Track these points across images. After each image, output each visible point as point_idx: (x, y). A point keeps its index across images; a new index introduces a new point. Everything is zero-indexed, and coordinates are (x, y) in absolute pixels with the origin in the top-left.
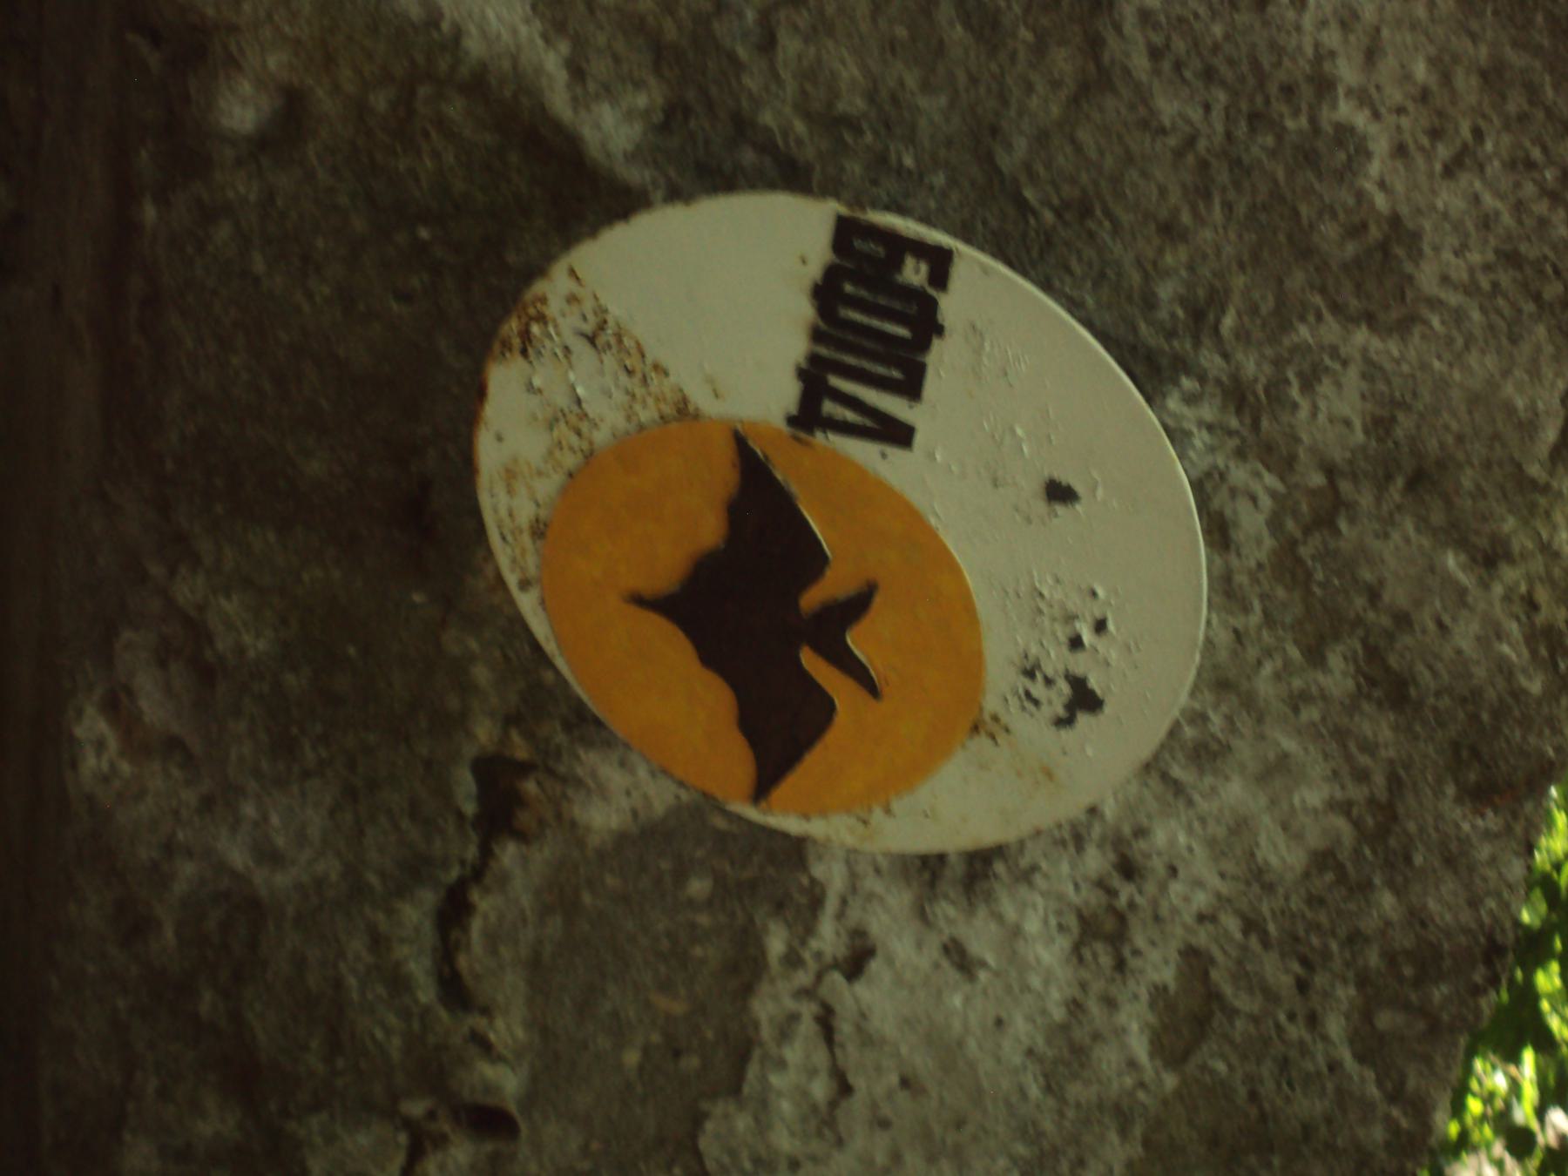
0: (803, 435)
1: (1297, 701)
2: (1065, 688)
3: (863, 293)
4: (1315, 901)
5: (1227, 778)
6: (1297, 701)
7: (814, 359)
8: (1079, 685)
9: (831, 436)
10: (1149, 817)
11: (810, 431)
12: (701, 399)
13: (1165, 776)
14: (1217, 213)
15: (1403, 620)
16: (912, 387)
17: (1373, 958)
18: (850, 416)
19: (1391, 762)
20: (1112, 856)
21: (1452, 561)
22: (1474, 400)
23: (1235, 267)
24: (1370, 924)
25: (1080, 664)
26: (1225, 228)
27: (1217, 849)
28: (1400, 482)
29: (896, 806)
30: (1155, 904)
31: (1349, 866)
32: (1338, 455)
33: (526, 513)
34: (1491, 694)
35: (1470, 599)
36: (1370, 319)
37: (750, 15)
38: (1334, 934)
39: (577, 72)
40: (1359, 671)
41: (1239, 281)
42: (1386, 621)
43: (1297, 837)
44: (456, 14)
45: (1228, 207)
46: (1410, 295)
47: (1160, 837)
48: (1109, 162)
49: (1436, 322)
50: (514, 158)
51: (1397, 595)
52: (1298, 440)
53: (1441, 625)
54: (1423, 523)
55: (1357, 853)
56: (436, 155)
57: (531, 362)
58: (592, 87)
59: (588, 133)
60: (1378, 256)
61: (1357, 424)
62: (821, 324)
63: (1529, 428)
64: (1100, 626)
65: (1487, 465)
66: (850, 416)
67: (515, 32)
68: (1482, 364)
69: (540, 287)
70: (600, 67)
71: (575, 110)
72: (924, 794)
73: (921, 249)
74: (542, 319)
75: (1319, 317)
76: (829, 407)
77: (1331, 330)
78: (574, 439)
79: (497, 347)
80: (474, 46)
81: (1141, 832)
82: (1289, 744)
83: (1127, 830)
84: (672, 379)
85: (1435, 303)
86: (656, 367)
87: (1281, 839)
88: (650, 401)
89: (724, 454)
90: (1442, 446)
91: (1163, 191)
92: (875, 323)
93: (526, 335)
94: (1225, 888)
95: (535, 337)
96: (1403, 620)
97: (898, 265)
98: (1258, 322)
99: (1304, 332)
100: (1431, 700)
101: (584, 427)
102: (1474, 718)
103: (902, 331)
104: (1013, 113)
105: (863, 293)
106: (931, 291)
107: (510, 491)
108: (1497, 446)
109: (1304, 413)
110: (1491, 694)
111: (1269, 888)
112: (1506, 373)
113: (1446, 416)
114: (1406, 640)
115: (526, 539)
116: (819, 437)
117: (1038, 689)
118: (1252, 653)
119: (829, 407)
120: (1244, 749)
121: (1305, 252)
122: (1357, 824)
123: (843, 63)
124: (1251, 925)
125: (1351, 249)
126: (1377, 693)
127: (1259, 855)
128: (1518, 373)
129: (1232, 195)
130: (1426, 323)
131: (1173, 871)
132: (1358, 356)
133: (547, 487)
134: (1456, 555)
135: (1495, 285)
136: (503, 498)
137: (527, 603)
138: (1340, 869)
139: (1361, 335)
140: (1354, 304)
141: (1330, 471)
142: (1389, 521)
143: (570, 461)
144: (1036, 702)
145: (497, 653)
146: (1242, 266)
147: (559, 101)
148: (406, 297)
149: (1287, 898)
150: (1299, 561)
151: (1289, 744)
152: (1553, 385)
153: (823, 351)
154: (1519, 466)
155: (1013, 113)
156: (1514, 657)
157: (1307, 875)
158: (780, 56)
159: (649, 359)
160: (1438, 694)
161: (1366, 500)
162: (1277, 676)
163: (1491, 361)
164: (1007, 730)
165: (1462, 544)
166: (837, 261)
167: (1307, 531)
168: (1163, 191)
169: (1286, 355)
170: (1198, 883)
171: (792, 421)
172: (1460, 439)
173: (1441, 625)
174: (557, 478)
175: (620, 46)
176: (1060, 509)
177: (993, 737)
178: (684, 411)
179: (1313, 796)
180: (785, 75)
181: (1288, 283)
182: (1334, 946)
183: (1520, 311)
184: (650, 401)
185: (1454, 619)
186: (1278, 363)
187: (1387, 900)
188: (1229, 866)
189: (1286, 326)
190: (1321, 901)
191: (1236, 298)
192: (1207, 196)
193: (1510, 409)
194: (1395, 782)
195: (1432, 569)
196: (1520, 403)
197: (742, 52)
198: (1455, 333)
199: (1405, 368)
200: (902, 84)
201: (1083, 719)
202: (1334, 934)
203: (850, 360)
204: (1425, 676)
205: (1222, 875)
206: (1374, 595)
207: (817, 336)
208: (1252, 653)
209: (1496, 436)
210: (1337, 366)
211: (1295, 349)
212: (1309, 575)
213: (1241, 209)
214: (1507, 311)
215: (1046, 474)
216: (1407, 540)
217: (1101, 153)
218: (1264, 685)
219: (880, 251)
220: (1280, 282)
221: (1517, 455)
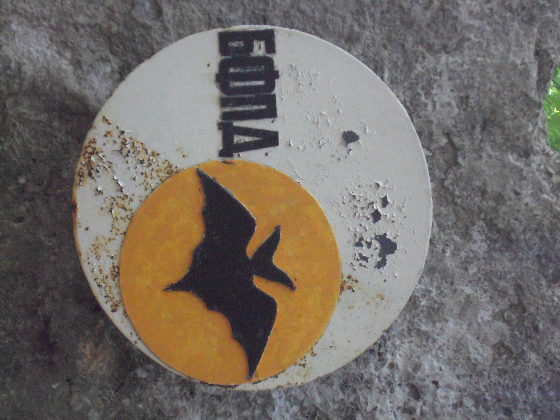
0: (228, 159)
1: (465, 264)
2: (376, 244)
3: (238, 70)
4: (503, 372)
5: (447, 321)
6: (465, 264)
7: (225, 116)
8: (382, 239)
9: (241, 154)
10: (418, 358)
11: (231, 156)
12: (179, 163)
13: (419, 332)
14: (369, 22)
15: (500, 199)
16: (271, 113)
17: (535, 394)
18: (247, 139)
19: (513, 279)
20: (407, 390)
21: (511, 158)
22: (498, 70)
23: (381, 48)
24: (529, 373)
25: (381, 228)
26: (373, 28)
27: (451, 363)
28: (478, 129)
29: (316, 351)
30: (433, 407)
31: (511, 346)
32: (449, 123)
33: (107, 265)
34: (546, 222)
35: (525, 174)
36: (445, 48)
37: (148, 5)
38: (515, 387)
39: (77, 63)
40: (488, 238)
41: (385, 53)
42: (491, 203)
43: (484, 340)
44: (16, 58)
45: (372, 15)
46: (459, 28)
47: (426, 366)
48: (317, 15)
49: (472, 36)
50: (56, 124)
51: (493, 187)
52: (431, 122)
53: (517, 193)
54: (494, 145)
55: (513, 336)
56: (20, 135)
57: (93, 178)
58: (85, 67)
59: (88, 93)
60: (441, 13)
61: (453, 103)
62: (224, 96)
63: (525, 74)
64: (385, 202)
65: (513, 100)
66: (247, 139)
67: (45, 55)
68: (498, 50)
69: (91, 135)
70: (86, 57)
71: (80, 84)
72: (327, 338)
73: (258, 35)
74: (95, 152)
75: (424, 57)
76: (238, 139)
77: (430, 61)
78: (123, 214)
79: (77, 178)
80: (28, 70)
81: (417, 367)
82: (468, 290)
83: (410, 370)
84: (162, 157)
85: (469, 28)
86: (153, 154)
87: (478, 344)
88: (155, 175)
89: (193, 182)
90: (491, 101)
91: (343, 19)
92: (248, 84)
93: (89, 164)
94: (460, 383)
95: (93, 162)
96: (500, 199)
97: (250, 48)
98: (399, 71)
99: (419, 68)
100: (522, 237)
101: (126, 203)
102: (542, 238)
103: (261, 83)
104: (271, 8)
105: (238, 70)
106: (269, 56)
107: (98, 257)
108: (515, 90)
109: (430, 107)
110: (546, 222)
111: (480, 374)
112: (508, 50)
113: (489, 85)
114: (503, 209)
115: (110, 282)
116: (236, 158)
117: (365, 252)
118: (440, 247)
119: (238, 139)
120: (449, 302)
121: (409, 24)
122: (508, 322)
123: (193, 11)
124: (479, 400)
125: (429, 14)
126: (498, 246)
127: (472, 357)
128: (513, 48)
129: (372, 9)
130: (469, 39)
131: (436, 383)
132: (445, 69)
133: (114, 247)
134: (512, 154)
135: (491, 10)
136: (92, 259)
137: (117, 318)
138: (509, 351)
139: (444, 58)
140: (437, 43)
141: (448, 135)
142: (479, 151)
143: (123, 226)
144: (366, 259)
145: (99, 400)
146: (385, 46)
147: (72, 84)
148: (20, 220)
149: (489, 377)
150: (447, 189)
151: (468, 290)
152: (529, 47)
153: (227, 110)
154: (526, 95)
155: (271, 8)
156: (551, 199)
157: (494, 360)
158: (165, 17)
159: (149, 152)
160: (524, 231)
161: (467, 143)
162: (453, 255)
163: (500, 46)
164: (356, 281)
165: (513, 148)
166: (223, 58)
167: (446, 173)
168: (343, 19)
169: (415, 81)
170: (449, 386)
171: (222, 154)
172: (498, 93)
173: (517, 193)
174: (119, 238)
175: (93, 45)
176: (351, 145)
177: (350, 288)
178: (171, 171)
179: (485, 315)
180: (170, 26)
181: (406, 46)
182: (517, 394)
183: (505, 18)
184: (155, 175)
185: (520, 187)
186: (411, 88)
187: (533, 356)
188: (460, 371)
189: (411, 69)
190: (505, 372)
191: (386, 62)
192: (363, 13)
193: (515, 66)
194: (519, 288)
195: (504, 166)
196: (518, 62)
197: (149, 23)
198: (481, 40)
199: (466, 67)
200: (221, 11)
201: (389, 258)
202: (515, 387)
203: (241, 109)
204: (517, 225)
205: (458, 377)
206: (483, 193)
207: (224, 103)
208: (440, 247)
209: (512, 85)
210: (437, 77)
211: (417, 77)
212: (452, 194)
213: (378, 16)
214: (500, 21)
215: (342, 131)
216: (490, 156)
217: (313, 12)
218: (450, 263)
219: (241, 44)
220: (403, 46)
221: (524, 90)
